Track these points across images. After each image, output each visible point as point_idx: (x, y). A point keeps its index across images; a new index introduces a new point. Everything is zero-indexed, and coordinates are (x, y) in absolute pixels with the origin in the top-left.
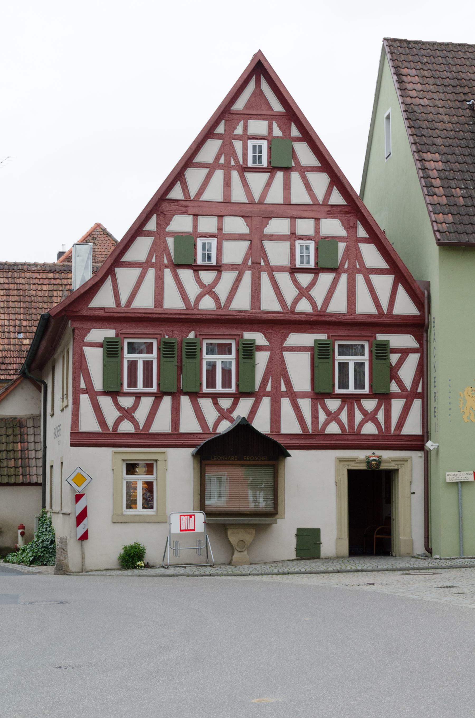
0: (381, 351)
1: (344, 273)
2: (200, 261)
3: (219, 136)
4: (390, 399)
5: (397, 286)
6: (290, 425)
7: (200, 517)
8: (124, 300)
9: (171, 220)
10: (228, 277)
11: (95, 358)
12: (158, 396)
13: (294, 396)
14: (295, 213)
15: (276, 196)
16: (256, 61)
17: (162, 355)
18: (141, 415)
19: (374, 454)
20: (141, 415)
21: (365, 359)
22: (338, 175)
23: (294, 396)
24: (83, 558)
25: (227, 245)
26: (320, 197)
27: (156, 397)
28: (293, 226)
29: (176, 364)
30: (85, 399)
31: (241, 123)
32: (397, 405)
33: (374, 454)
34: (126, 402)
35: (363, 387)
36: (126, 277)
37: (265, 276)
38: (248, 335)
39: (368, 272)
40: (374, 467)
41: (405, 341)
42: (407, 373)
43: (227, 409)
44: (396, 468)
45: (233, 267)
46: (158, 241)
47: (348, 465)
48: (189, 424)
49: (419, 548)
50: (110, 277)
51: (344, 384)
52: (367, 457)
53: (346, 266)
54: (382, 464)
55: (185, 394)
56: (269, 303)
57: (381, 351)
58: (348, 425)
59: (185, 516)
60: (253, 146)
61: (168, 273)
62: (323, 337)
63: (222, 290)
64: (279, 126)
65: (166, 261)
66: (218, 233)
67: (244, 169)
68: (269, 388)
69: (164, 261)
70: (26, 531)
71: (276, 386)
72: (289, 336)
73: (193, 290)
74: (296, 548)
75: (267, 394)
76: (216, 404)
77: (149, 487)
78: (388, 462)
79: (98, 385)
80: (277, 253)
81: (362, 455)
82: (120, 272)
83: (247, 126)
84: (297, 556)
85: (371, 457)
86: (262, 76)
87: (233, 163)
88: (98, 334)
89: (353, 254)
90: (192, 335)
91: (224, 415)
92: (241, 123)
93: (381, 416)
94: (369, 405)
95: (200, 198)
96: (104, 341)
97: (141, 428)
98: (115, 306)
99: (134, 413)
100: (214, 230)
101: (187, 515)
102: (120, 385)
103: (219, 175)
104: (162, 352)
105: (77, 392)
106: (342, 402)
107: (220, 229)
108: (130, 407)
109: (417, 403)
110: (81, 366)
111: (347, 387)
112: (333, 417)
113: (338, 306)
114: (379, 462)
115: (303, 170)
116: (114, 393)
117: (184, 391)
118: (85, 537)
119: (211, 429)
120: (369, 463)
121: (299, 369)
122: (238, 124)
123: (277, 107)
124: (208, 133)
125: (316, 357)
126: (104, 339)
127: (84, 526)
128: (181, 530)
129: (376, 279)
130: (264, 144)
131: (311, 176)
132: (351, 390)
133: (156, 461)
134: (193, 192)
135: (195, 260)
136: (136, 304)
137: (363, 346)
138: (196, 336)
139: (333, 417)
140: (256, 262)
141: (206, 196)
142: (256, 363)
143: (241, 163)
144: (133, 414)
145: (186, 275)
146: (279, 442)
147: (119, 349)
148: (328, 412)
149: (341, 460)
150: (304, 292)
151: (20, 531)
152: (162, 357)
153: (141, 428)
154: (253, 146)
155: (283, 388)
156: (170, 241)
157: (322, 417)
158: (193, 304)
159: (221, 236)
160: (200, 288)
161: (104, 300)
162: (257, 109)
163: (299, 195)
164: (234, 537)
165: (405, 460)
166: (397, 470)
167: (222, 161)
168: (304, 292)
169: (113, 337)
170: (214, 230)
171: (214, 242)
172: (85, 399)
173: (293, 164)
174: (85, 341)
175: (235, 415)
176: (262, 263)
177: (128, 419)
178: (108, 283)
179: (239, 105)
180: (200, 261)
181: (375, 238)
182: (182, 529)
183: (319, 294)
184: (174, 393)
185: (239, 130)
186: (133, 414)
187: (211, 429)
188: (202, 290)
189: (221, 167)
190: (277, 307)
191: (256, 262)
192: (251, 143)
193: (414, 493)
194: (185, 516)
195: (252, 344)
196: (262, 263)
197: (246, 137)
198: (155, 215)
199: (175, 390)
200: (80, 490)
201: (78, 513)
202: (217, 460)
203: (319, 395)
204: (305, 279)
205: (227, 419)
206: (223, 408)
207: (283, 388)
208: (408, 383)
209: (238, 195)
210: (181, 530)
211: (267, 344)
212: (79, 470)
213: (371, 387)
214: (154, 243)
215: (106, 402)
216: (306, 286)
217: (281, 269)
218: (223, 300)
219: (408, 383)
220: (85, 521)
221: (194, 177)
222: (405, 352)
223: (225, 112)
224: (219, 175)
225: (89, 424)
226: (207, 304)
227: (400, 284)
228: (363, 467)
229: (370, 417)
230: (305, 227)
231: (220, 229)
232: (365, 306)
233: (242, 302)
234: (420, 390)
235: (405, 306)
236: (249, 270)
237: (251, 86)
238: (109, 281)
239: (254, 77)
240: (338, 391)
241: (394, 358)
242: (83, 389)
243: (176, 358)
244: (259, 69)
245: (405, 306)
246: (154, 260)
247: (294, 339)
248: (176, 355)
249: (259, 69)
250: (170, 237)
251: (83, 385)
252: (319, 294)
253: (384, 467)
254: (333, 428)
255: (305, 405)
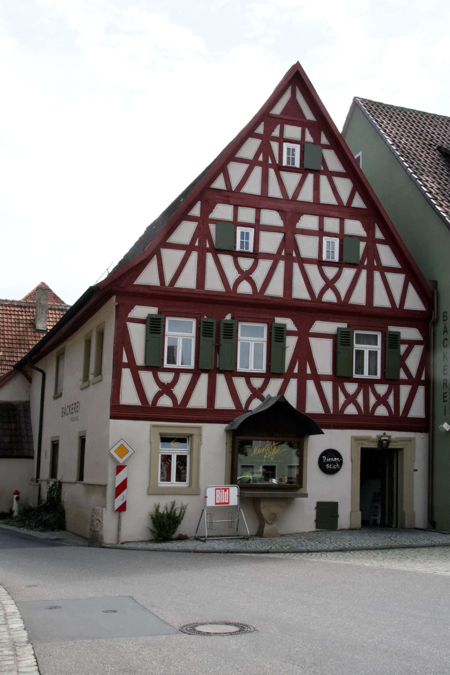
0: (392, 342)
1: (364, 269)
2: (238, 248)
3: (258, 136)
4: (399, 385)
5: (408, 284)
6: (313, 406)
7: (234, 491)
8: (168, 279)
9: (213, 208)
10: (264, 265)
11: (137, 334)
12: (196, 373)
13: (318, 379)
14: (325, 212)
15: (307, 195)
16: (295, 71)
17: (201, 333)
18: (179, 391)
19: (384, 434)
20: (179, 391)
21: (378, 348)
22: (363, 180)
23: (318, 379)
24: (119, 529)
25: (263, 235)
26: (345, 200)
27: (194, 374)
28: (321, 224)
29: (214, 343)
30: (126, 373)
31: (278, 127)
32: (405, 390)
33: (384, 434)
34: (166, 378)
35: (376, 374)
36: (171, 258)
37: (296, 267)
38: (279, 320)
39: (384, 270)
40: (384, 446)
41: (409, 333)
42: (413, 362)
43: (258, 388)
44: (401, 447)
45: (267, 256)
46: (202, 226)
47: (362, 444)
48: (224, 401)
49: (420, 519)
50: (155, 256)
51: (360, 370)
52: (379, 437)
53: (366, 263)
54: (390, 444)
55: (221, 372)
56: (300, 292)
57: (392, 342)
58: (364, 407)
59: (220, 489)
60: (288, 148)
61: (209, 257)
62: (344, 325)
63: (259, 276)
64: (311, 133)
65: (208, 246)
66: (255, 223)
67: (279, 168)
68: (296, 371)
69: (206, 245)
70: (20, 496)
71: (302, 369)
72: (315, 324)
73: (232, 275)
74: (315, 521)
75: (295, 376)
76: (248, 383)
77: (182, 460)
78: (396, 442)
79: (140, 360)
80: (307, 246)
81: (374, 434)
82: (166, 253)
83: (283, 130)
84: (317, 528)
85: (382, 437)
86: (297, 87)
87: (270, 162)
88: (141, 311)
89: (371, 253)
90: (228, 317)
91: (256, 393)
92: (278, 127)
93: (391, 400)
94: (382, 389)
95: (240, 190)
96: (147, 317)
97: (179, 403)
98: (159, 285)
99: (173, 388)
100: (252, 220)
101: (222, 489)
102: (161, 360)
103: (257, 171)
104: (201, 331)
105: (118, 367)
106: (359, 386)
107: (258, 219)
108: (169, 382)
109: (421, 390)
110: (123, 340)
111: (362, 373)
112: (351, 399)
113: (359, 298)
114: (388, 442)
115: (330, 175)
116: (155, 368)
117: (220, 369)
118: (123, 508)
119: (244, 407)
120: (380, 442)
121: (322, 354)
122: (275, 128)
123: (309, 115)
124: (248, 133)
125: (339, 342)
126: (147, 316)
127: (122, 497)
128: (216, 504)
129: (390, 276)
130: (297, 148)
131: (337, 180)
132: (366, 375)
133: (191, 435)
134: (234, 184)
135: (235, 247)
136: (180, 284)
137: (376, 336)
138: (233, 318)
139: (351, 399)
140: (289, 253)
141: (246, 189)
142: (286, 346)
143: (277, 162)
144: (172, 389)
145: (226, 260)
146: (315, 421)
147: (162, 326)
148: (376, 395)
149: (356, 439)
150: (330, 284)
151: (15, 496)
152: (201, 337)
153: (179, 403)
154: (288, 148)
155: (309, 371)
156: (212, 227)
157: (342, 399)
158: (231, 288)
159: (258, 227)
160: (239, 273)
161: (149, 277)
162: (292, 115)
163: (326, 197)
164: (266, 510)
165: (410, 440)
166: (402, 449)
167: (261, 158)
168: (330, 284)
169: (155, 313)
170: (252, 220)
171: (251, 231)
172: (126, 373)
173: (322, 169)
174: (129, 316)
175: (265, 394)
176: (294, 255)
177: (166, 394)
178: (154, 263)
179: (277, 110)
180: (238, 248)
181: (392, 240)
182: (217, 502)
183: (342, 286)
184: (212, 370)
185: (276, 133)
186: (172, 389)
187: (244, 407)
188: (240, 275)
189: (260, 164)
190: (306, 296)
191: (289, 253)
192: (286, 146)
193: (416, 470)
194: (220, 489)
195: (283, 328)
196: (294, 255)
197: (281, 140)
198: (199, 202)
199: (212, 368)
200: (121, 461)
201: (117, 484)
202: (250, 436)
203: (339, 378)
204: (331, 272)
205: (258, 398)
206: (255, 387)
207: (309, 371)
208: (413, 370)
209: (274, 191)
210: (216, 504)
211: (295, 329)
212: (122, 442)
213: (383, 373)
214: (198, 228)
215: (146, 377)
216: (332, 278)
217: (310, 261)
218: (259, 286)
219: (413, 370)
220: (124, 493)
221: (236, 171)
222: (411, 344)
223: (265, 116)
224: (257, 171)
225: (128, 397)
226: (245, 288)
227: (410, 283)
228: (374, 445)
229: (381, 400)
230: (331, 224)
231: (258, 219)
232: (381, 300)
233: (276, 289)
234: (423, 378)
235: (414, 302)
236: (282, 260)
237: (287, 96)
238: (154, 260)
239: (290, 87)
240: (355, 376)
241: (403, 348)
242: (125, 363)
243: (214, 337)
244: (297, 79)
245: (414, 302)
246: (197, 244)
247: (319, 326)
248: (214, 335)
249: (297, 79)
250: (212, 223)
251: (125, 360)
252: (342, 286)
253: (391, 446)
254: (351, 410)
255: (327, 387)
